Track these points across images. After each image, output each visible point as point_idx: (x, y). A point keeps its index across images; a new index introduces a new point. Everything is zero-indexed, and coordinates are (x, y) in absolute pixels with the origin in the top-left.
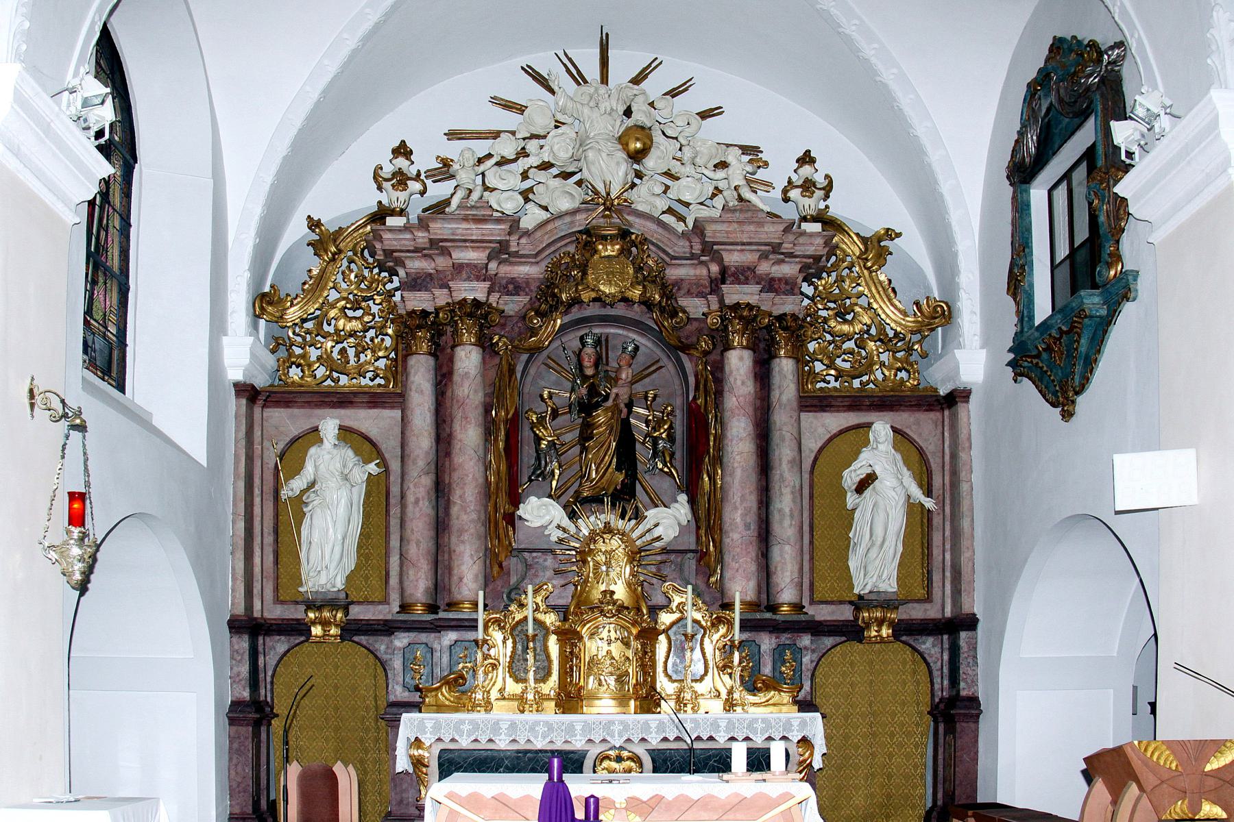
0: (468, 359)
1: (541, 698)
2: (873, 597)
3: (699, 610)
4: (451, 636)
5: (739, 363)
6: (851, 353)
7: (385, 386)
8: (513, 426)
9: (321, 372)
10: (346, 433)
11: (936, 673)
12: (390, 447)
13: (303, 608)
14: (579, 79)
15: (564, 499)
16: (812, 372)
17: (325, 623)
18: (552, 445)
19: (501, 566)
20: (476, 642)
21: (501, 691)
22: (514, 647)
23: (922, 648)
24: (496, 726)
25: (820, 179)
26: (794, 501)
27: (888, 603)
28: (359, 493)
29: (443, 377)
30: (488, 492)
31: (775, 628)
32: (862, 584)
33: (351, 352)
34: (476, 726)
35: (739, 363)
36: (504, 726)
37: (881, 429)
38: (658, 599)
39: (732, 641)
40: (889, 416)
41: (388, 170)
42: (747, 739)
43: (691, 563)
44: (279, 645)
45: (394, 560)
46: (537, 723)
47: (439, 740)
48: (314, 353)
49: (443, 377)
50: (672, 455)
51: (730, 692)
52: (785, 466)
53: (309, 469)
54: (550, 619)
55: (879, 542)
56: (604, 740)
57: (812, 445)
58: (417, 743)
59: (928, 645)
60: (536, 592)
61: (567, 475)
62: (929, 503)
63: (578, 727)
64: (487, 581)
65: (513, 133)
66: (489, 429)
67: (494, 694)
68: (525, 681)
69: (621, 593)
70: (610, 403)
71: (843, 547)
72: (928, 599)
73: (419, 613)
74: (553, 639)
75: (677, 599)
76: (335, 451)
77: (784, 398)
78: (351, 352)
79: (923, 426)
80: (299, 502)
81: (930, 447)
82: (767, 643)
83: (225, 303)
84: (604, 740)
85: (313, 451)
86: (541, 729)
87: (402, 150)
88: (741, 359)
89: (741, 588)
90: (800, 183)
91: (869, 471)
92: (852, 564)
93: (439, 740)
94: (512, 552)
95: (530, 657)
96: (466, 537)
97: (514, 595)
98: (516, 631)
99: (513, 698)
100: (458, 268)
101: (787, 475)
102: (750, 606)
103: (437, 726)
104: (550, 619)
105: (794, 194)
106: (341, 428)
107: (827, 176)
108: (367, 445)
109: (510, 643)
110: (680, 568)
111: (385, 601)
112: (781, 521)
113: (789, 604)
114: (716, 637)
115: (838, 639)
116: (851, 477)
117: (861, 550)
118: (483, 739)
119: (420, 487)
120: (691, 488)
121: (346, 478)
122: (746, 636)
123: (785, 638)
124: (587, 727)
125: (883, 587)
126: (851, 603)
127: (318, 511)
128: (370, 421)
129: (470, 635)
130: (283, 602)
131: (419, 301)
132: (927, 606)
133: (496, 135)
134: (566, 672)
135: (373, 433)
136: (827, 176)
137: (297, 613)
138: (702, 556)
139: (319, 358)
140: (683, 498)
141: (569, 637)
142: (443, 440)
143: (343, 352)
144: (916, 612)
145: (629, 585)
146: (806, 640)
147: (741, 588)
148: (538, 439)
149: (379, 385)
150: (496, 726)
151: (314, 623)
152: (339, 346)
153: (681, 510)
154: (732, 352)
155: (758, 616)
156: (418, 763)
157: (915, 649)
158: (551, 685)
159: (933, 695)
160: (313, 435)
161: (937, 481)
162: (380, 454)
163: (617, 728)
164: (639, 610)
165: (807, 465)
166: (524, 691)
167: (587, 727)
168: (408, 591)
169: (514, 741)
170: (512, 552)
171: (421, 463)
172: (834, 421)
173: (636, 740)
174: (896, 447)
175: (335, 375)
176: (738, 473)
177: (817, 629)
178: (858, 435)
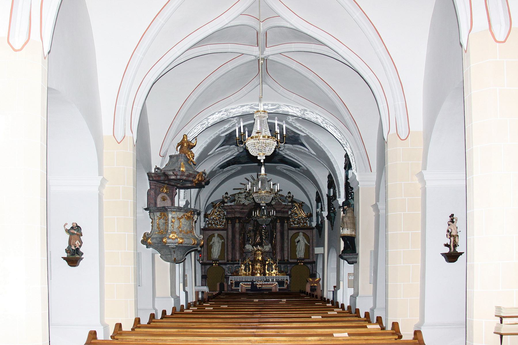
0: (237, 225)
1: (249, 274)
2: (300, 259)
3: (272, 261)
4: (236, 265)
5: (278, 225)
6: (297, 221)
7: (224, 227)
8: (244, 234)
9: (214, 225)
10: (219, 235)
11: (310, 270)
12: (225, 236)
13: (212, 261)
14: (254, 179)
15: (252, 244)
16: (291, 224)
17: (216, 263)
18: (250, 236)
19: (242, 255)
20: (239, 266)
21: (243, 273)
22: (245, 267)
23: (308, 266)
24: (243, 278)
25: (291, 195)
26: (287, 245)
27: (303, 259)
28: (220, 244)
29: (233, 227)
30: (240, 244)
31: (283, 264)
32: (298, 257)
33: (218, 222)
34: (234, 278)
35: (278, 225)
36: (244, 278)
37: (301, 234)
38: (266, 259)
39: (277, 266)
40: (303, 231)
41: (224, 196)
42: (263, 280)
43: (271, 254)
44: (208, 267)
45: (226, 254)
46: (248, 278)
47: (235, 280)
48: (213, 223)
49: (233, 227)
50: (269, 237)
51: (276, 273)
52: (286, 239)
53: (213, 240)
54: (250, 263)
55: (300, 250)
56: (258, 280)
57: (290, 235)
58: (232, 280)
59: (309, 266)
60: (248, 259)
61: (252, 240)
62: (309, 244)
63: (233, 278)
64: (240, 257)
65: (243, 189)
66: (240, 235)
67: (242, 274)
68: (247, 271)
69: (260, 258)
70: (259, 230)
71: (295, 251)
72: (309, 259)
73: (230, 262)
74: (250, 266)
75: (269, 260)
76: (217, 238)
77: (286, 229)
78: (218, 222)
79: (308, 233)
80: (211, 246)
81: (309, 235)
82: (282, 266)
83: (180, 196)
84: (258, 280)
85: (213, 238)
86: (249, 278)
87: (227, 193)
88: (279, 224)
89: (279, 258)
90: (288, 196)
91: (299, 240)
92: (297, 253)
93: (235, 280)
94: (244, 252)
95: (247, 268)
96: (237, 251)
97: (244, 259)
98: (245, 265)
99: (245, 274)
100: (235, 211)
101: (286, 241)
102: (280, 260)
103: (234, 278)
104: (250, 263)
105: (287, 198)
106: (218, 234)
107: (293, 195)
108: (221, 236)
109: (244, 267)
110: (270, 255)
111: (224, 260)
112: (285, 248)
113: (286, 260)
114: (274, 265)
115: (295, 265)
116: (296, 240)
117: (298, 252)
118: (236, 280)
119: (230, 243)
120: (271, 242)
121: (218, 242)
122: (279, 265)
123: (285, 265)
124: (255, 278)
125: (301, 257)
126: (297, 259)
127: (215, 247)
128: (221, 233)
129: (238, 265)
130: (208, 260)
131: (229, 216)
132: (309, 260)
133: (241, 189)
134: (252, 271)
135: (222, 235)
136: (293, 195)
137: (211, 262)
138: (273, 253)
139: (214, 223)
140: (270, 244)
141: (253, 266)
142: (234, 236)
143: (217, 222)
144: (307, 260)
145: (261, 258)
146: (289, 265)
147: (279, 258)
148: (248, 235)
149: (223, 227)
150: (243, 278)
151: (214, 263)
152: (217, 221)
153: (270, 246)
154: (277, 223)
155: (281, 262)
156: (232, 283)
157: (307, 266)
158: (250, 272)
159: (310, 273)
160: (213, 235)
161: (310, 242)
162: (224, 239)
163: (260, 278)
164: (263, 261)
165: (290, 238)
166: (246, 273)
167: (255, 278)
168: (229, 258)
169: (245, 280)
170: (244, 252)
171: (230, 240)
172: (294, 232)
173: (262, 280)
174: (303, 236)
175: (216, 226)
176: (278, 241)
177: (291, 263)
178: (297, 235)
